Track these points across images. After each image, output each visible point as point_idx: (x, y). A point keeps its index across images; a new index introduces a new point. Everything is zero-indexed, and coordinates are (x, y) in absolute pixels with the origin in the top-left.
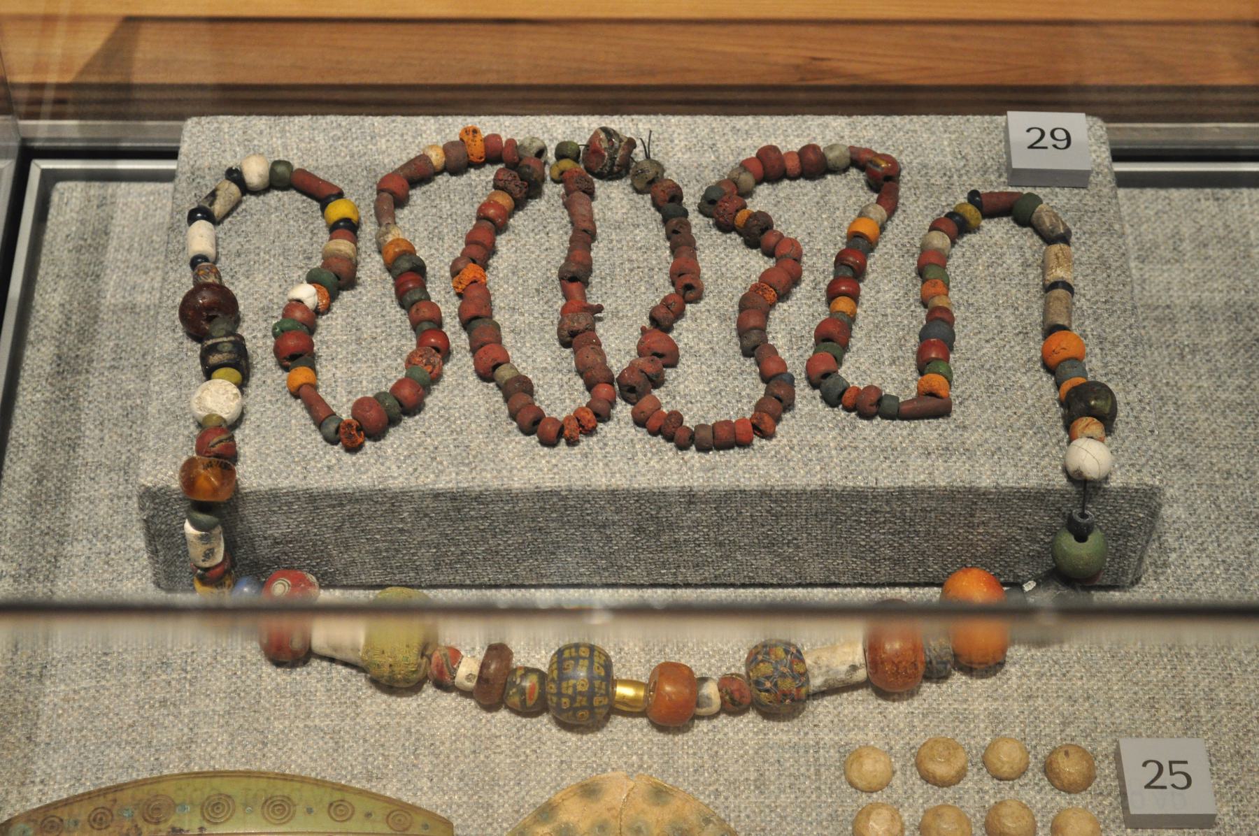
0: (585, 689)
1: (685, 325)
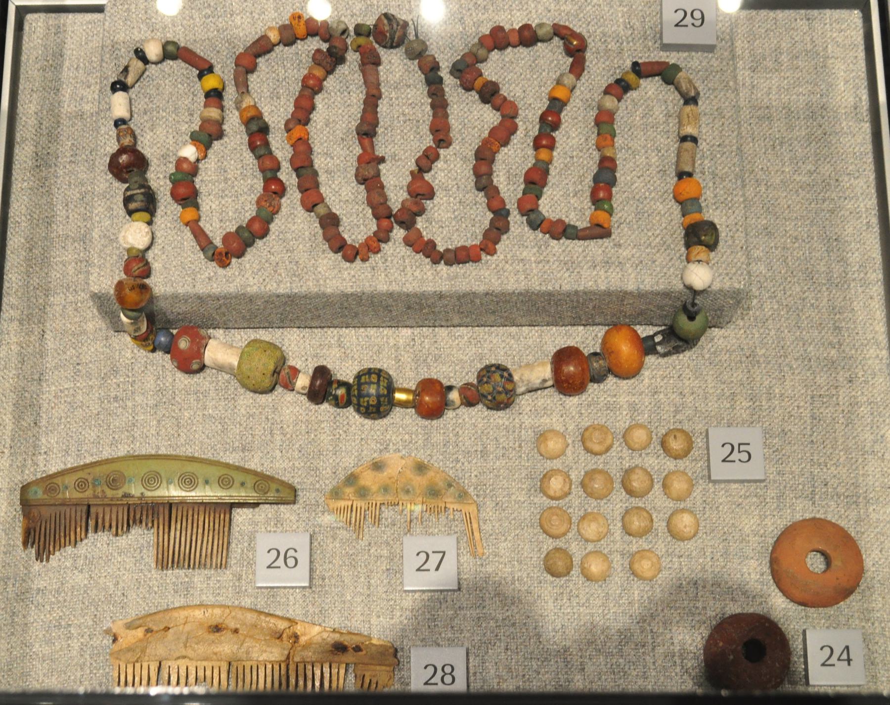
1: (439, 166)
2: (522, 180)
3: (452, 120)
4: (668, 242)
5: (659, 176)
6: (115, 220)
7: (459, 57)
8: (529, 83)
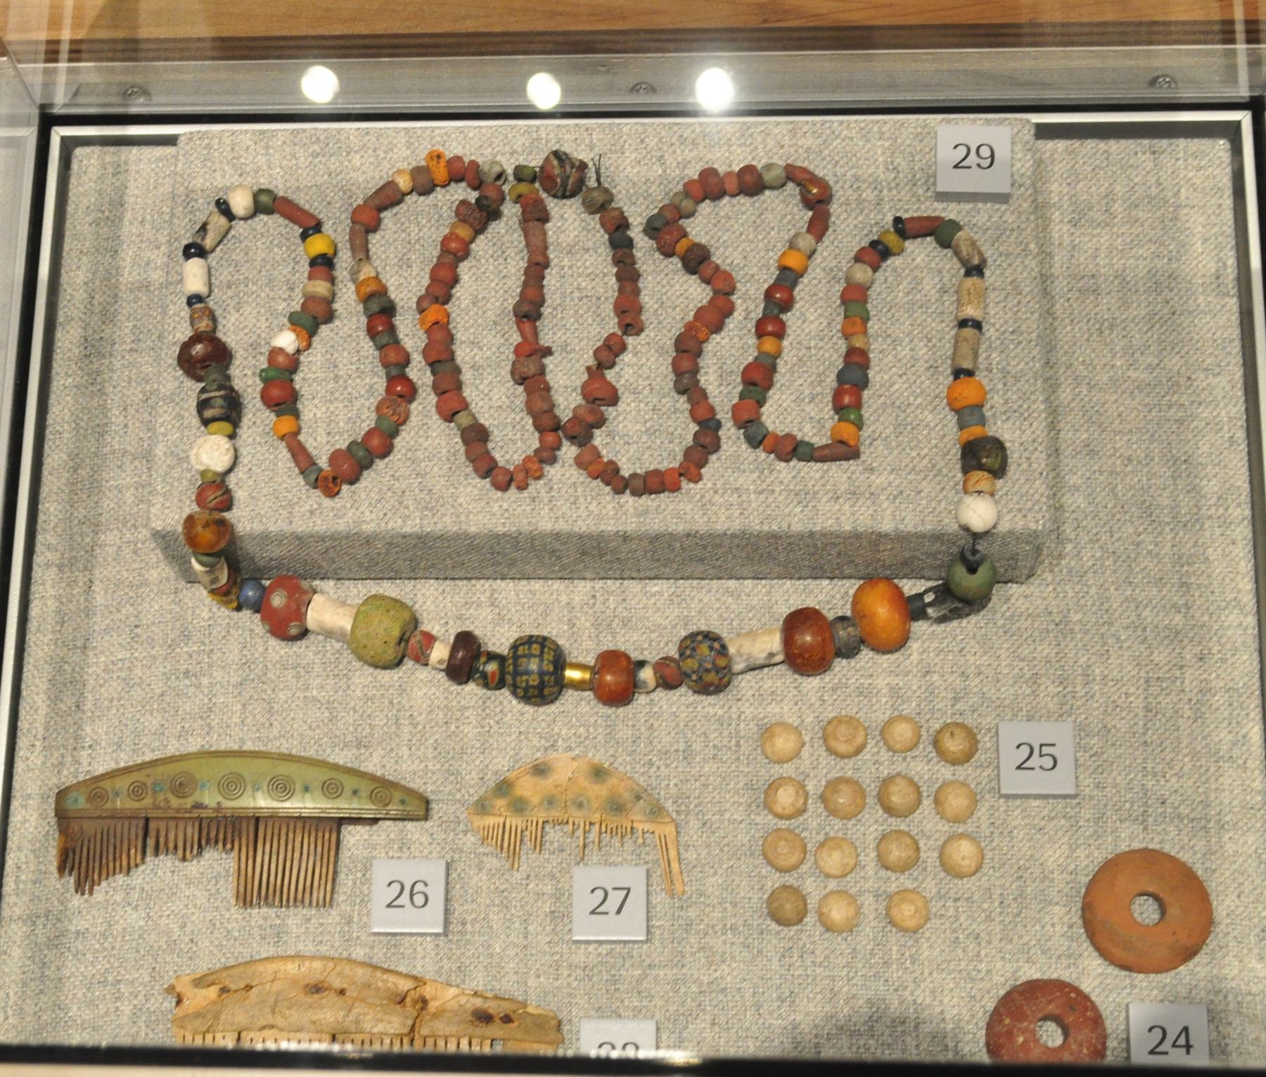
0: (536, 683)
2: (739, 380)
3: (645, 298)
4: (938, 467)
5: (928, 374)
6: (186, 432)
7: (656, 211)
8: (753, 246)
